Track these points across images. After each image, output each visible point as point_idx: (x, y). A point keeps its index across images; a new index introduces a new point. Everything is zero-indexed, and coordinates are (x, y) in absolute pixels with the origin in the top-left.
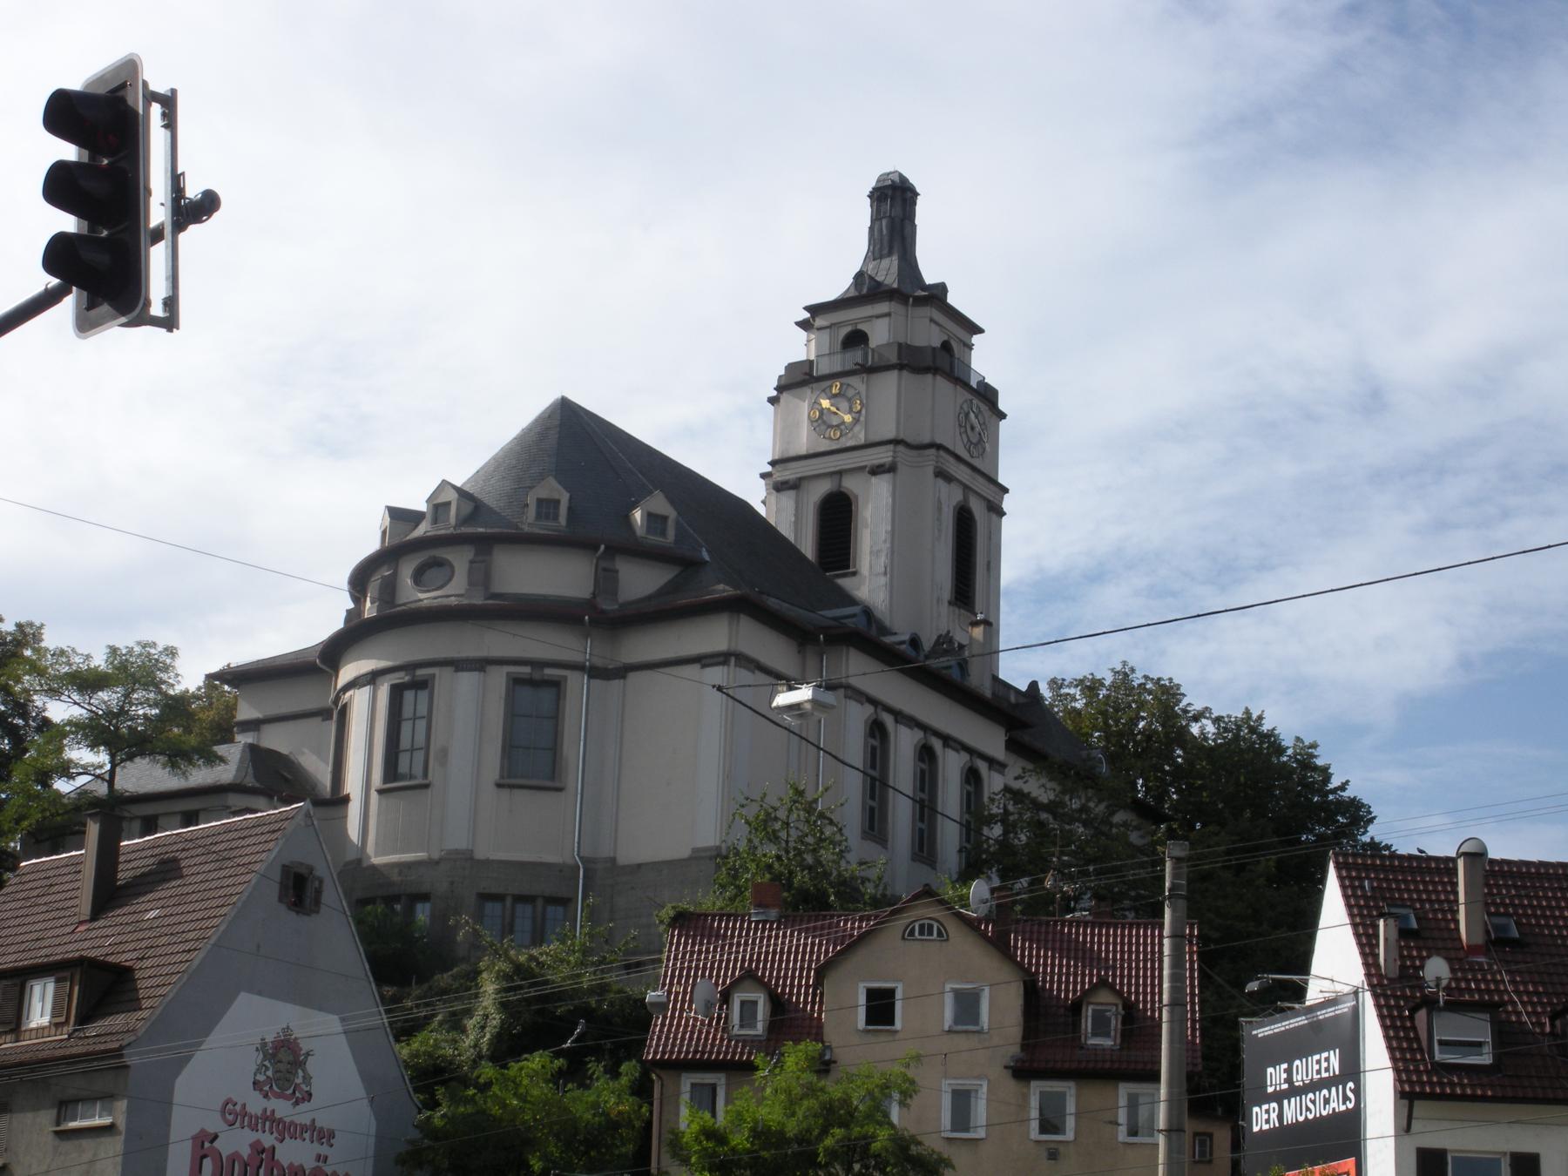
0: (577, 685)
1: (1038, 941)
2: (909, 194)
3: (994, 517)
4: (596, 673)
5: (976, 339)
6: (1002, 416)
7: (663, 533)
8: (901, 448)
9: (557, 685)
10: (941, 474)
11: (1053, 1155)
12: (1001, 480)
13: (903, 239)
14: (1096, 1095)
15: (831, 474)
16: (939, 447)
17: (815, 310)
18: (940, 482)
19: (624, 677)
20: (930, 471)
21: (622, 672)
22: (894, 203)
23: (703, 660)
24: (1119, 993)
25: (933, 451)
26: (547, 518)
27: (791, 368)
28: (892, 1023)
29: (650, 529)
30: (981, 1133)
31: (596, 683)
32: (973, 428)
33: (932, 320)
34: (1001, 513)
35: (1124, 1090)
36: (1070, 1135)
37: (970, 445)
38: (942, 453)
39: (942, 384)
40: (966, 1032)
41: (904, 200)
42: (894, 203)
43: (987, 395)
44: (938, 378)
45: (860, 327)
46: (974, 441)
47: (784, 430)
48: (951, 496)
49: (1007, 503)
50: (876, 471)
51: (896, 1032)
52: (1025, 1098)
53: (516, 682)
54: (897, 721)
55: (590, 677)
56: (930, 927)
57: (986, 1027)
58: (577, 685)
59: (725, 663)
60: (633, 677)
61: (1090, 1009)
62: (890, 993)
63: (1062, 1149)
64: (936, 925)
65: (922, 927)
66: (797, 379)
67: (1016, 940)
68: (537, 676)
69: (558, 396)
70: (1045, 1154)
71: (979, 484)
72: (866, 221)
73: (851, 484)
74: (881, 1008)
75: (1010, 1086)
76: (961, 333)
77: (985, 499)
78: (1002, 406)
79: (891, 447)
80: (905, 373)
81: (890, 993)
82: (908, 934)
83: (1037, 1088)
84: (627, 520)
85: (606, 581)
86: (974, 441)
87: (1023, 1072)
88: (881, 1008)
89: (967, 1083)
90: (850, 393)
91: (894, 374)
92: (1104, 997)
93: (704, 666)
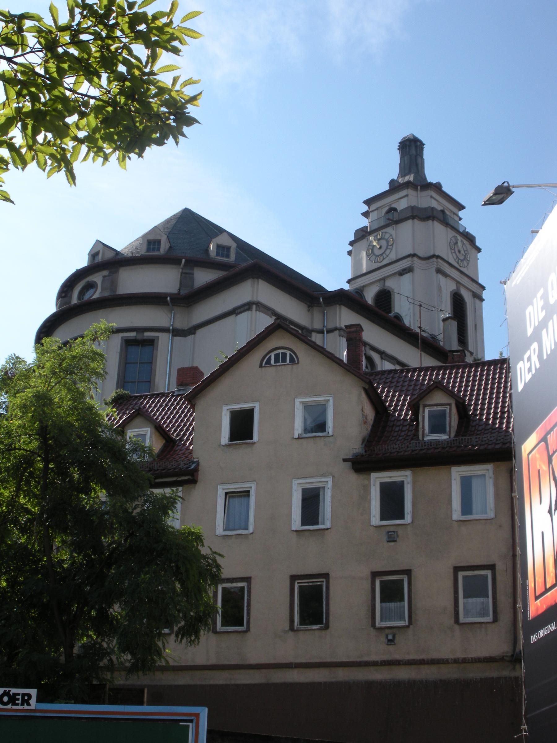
0: (164, 339)
1: (401, 391)
2: (419, 143)
3: (477, 301)
4: (177, 333)
5: (461, 214)
6: (479, 250)
7: (228, 256)
8: (415, 259)
9: (151, 342)
10: (439, 271)
11: (392, 538)
12: (480, 282)
13: (417, 165)
14: (431, 477)
15: (380, 280)
16: (438, 257)
17: (368, 202)
18: (440, 276)
19: (194, 333)
20: (433, 270)
21: (192, 330)
22: (411, 149)
23: (235, 312)
24: (451, 394)
25: (435, 259)
26: (154, 250)
27: (357, 232)
28: (251, 438)
29: (218, 254)
30: (328, 525)
31: (177, 339)
32: (459, 252)
33: (431, 197)
34: (482, 300)
35: (457, 473)
36: (408, 518)
37: (458, 260)
38: (439, 260)
39: (438, 227)
40: (315, 437)
41: (416, 147)
42: (411, 149)
43: (470, 239)
44: (435, 222)
45: (393, 206)
46: (462, 258)
47: (356, 264)
48: (448, 287)
49: (485, 295)
50: (402, 273)
51: (254, 443)
52: (366, 489)
53: (128, 343)
54: (382, 358)
55: (174, 336)
56: (284, 355)
57: (331, 433)
58: (164, 339)
59: (249, 309)
60: (199, 332)
61: (427, 410)
62: (250, 413)
63: (400, 532)
64: (288, 353)
65: (277, 356)
66: (361, 235)
67: (406, 415)
68: (140, 337)
69: (184, 208)
70: (385, 538)
71: (465, 281)
72: (398, 161)
73: (390, 284)
74: (242, 427)
75: (353, 478)
76: (454, 210)
77: (471, 291)
78: (478, 243)
79: (410, 259)
80: (416, 220)
81: (250, 413)
82: (265, 363)
83: (377, 479)
84: (207, 250)
85: (186, 278)
86: (462, 258)
87: (362, 464)
88: (242, 427)
89: (313, 482)
90: (387, 236)
91: (410, 222)
92: (439, 398)
93: (237, 314)
